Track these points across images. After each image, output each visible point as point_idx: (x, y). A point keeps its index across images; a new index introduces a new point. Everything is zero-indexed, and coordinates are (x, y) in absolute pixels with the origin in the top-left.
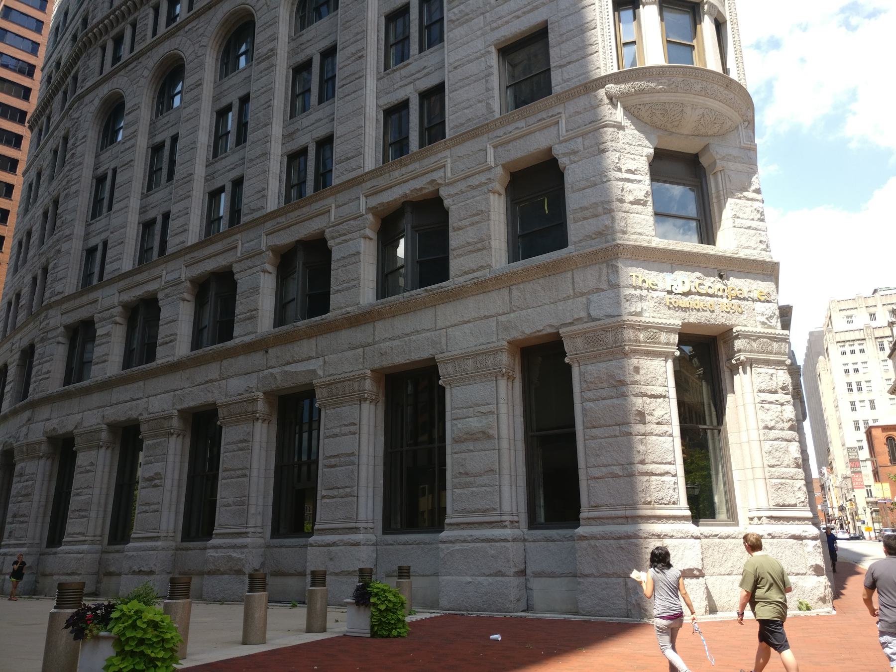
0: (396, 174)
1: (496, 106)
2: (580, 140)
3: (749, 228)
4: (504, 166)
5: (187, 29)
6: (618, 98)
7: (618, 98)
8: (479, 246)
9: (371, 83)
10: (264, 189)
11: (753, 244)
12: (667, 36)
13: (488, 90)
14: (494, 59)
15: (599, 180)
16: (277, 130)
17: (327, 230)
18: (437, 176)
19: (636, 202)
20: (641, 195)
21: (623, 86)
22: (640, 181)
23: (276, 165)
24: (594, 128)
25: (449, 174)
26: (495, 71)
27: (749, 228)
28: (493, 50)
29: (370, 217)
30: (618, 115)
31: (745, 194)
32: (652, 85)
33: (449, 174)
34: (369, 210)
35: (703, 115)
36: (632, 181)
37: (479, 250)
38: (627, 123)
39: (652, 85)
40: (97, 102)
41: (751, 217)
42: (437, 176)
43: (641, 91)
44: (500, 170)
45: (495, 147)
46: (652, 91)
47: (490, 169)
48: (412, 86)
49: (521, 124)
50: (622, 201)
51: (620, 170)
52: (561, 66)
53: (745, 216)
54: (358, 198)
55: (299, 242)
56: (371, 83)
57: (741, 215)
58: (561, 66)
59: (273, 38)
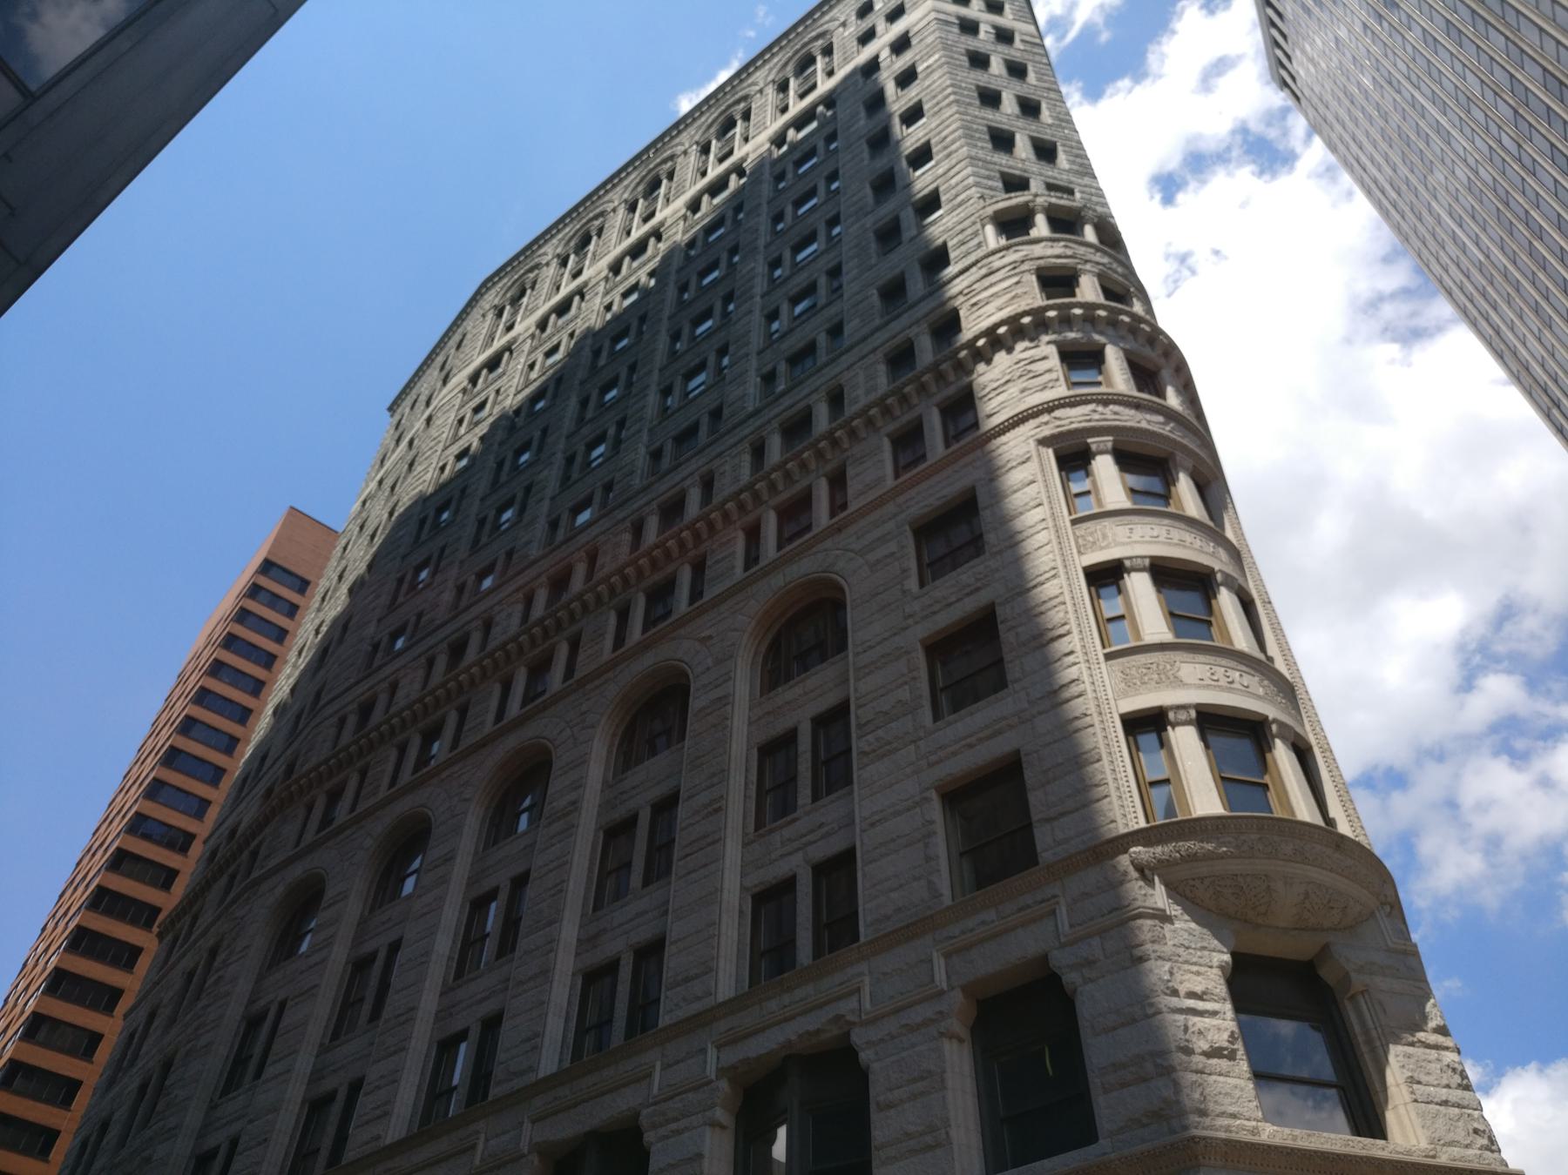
0: (773, 1005)
1: (944, 884)
2: (1096, 941)
3: (1445, 1103)
4: (964, 989)
5: (444, 775)
6: (1153, 870)
7: (1153, 870)
8: (929, 1139)
9: (733, 851)
10: (537, 1035)
11: (1460, 1135)
12: (1220, 770)
13: (928, 859)
14: (935, 810)
15: (1140, 1011)
16: (569, 932)
17: (644, 1112)
18: (846, 1007)
19: (1215, 1053)
20: (1222, 1039)
21: (1159, 849)
22: (1214, 1014)
23: (562, 992)
24: (1117, 928)
25: (867, 1005)
26: (939, 827)
27: (1445, 1103)
28: (933, 795)
29: (724, 1085)
30: (1158, 897)
31: (1421, 1035)
32: (1210, 846)
33: (867, 1005)
34: (722, 1072)
35: (1307, 895)
36: (1201, 1013)
37: (930, 1148)
38: (1175, 910)
39: (1210, 846)
40: (280, 890)
41: (1445, 1082)
42: (846, 1007)
43: (1192, 858)
44: (957, 997)
45: (947, 956)
46: (1210, 857)
47: (941, 993)
48: (800, 854)
49: (991, 915)
50: (1188, 1051)
51: (1175, 993)
52: (1048, 820)
53: (1431, 1079)
54: (703, 1051)
55: (594, 1136)
56: (733, 851)
57: (1424, 1078)
58: (1048, 820)
59: (578, 785)
